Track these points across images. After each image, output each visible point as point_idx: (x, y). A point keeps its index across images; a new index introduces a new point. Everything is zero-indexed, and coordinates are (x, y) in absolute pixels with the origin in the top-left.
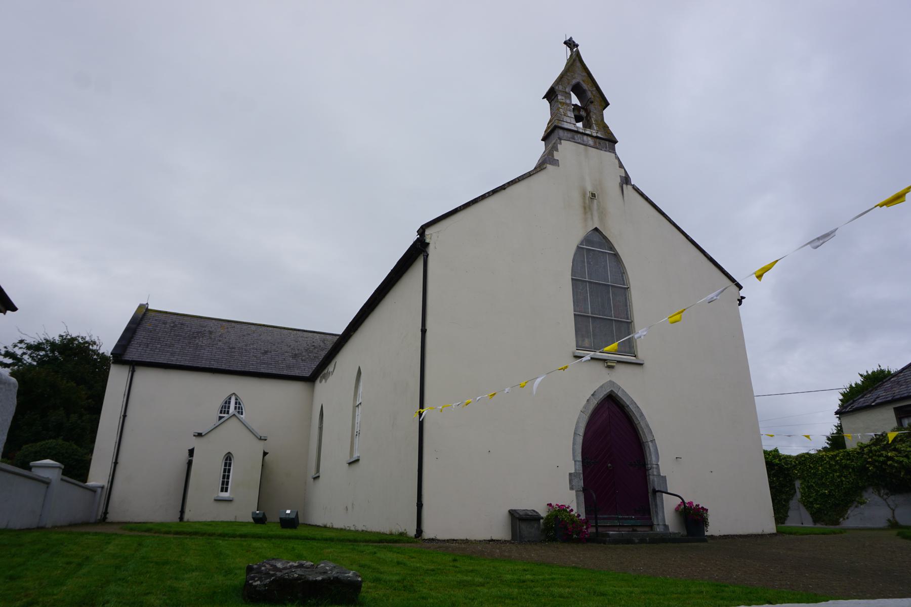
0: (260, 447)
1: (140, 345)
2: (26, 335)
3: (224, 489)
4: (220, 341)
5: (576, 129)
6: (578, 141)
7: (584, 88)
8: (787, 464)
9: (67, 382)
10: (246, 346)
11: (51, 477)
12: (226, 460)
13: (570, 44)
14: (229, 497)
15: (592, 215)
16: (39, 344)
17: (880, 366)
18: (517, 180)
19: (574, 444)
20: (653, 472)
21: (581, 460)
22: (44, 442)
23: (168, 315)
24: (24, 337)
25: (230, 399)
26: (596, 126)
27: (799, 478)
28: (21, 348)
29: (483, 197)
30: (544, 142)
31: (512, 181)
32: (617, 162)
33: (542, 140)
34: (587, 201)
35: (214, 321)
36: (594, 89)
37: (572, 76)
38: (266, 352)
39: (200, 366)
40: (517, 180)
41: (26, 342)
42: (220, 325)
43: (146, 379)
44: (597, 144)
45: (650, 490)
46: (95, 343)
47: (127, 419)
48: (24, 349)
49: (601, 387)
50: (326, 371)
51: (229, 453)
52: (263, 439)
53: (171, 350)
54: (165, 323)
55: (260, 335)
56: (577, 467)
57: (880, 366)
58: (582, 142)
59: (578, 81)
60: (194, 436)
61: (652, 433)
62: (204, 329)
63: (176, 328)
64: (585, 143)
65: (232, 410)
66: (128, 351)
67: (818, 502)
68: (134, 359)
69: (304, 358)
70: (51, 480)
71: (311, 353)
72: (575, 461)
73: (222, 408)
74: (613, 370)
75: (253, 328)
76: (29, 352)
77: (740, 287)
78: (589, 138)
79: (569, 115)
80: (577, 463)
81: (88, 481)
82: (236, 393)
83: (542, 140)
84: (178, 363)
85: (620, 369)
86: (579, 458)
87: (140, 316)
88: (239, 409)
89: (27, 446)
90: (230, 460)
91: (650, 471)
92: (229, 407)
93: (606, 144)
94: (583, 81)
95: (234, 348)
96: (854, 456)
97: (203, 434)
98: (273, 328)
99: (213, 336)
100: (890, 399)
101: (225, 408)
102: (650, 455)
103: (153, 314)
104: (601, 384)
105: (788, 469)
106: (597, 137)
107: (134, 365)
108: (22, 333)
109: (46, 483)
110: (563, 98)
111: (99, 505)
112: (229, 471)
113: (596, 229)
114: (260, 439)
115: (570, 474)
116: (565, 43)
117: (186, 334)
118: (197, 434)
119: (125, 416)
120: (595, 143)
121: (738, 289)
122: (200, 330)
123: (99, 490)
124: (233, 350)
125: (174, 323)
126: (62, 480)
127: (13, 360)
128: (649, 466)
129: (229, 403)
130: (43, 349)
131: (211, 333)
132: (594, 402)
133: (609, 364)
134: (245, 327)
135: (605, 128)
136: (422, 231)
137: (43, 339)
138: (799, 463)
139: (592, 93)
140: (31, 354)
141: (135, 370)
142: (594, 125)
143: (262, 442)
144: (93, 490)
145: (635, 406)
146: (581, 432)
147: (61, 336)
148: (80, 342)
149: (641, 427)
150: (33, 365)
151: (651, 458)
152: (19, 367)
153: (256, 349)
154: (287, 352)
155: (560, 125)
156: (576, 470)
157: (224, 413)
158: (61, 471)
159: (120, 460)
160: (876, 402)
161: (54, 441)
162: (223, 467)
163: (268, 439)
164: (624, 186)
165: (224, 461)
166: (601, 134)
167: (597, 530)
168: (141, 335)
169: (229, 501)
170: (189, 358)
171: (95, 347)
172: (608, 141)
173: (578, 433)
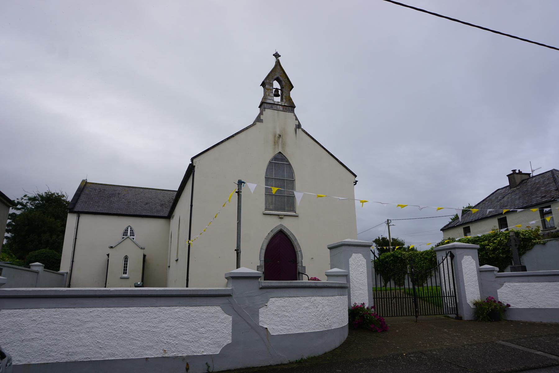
0: (141, 253)
1: (82, 202)
2: (28, 192)
3: (125, 272)
4: (123, 198)
5: (273, 103)
6: (274, 109)
7: (281, 80)
8: (404, 257)
9: (50, 218)
10: (137, 200)
11: (39, 270)
12: (125, 259)
13: (277, 55)
14: (127, 277)
15: (278, 146)
16: (35, 197)
17: (469, 204)
18: (240, 132)
19: (260, 253)
20: (299, 265)
21: (264, 260)
22: (40, 251)
23: (97, 185)
24: (26, 194)
25: (128, 228)
26: (285, 100)
27: (409, 264)
28: (25, 200)
29: (222, 142)
30: (259, 108)
31: (237, 133)
32: (294, 117)
33: (259, 107)
34: (276, 139)
35: (121, 187)
36: (286, 79)
37: (275, 74)
38: (147, 204)
39: (111, 213)
40: (240, 132)
41: (27, 196)
42: (124, 190)
43: (84, 219)
44: (285, 109)
45: (298, 273)
46: (64, 196)
47: (77, 240)
48: (27, 200)
49: (276, 227)
50: (173, 215)
51: (126, 256)
52: (143, 249)
53: (98, 204)
54: (95, 190)
55: (145, 194)
56: (261, 263)
57: (469, 204)
58: (276, 109)
59: (278, 76)
60: (109, 248)
61: (300, 247)
62: (116, 192)
63: (101, 192)
64: (278, 109)
65: (129, 234)
66: (76, 206)
67: (415, 276)
68: (79, 210)
69: (166, 206)
70: (39, 271)
71: (170, 203)
72: (260, 261)
73: (124, 233)
74: (283, 219)
75: (142, 190)
76: (30, 202)
77: (356, 176)
78: (280, 107)
79: (271, 95)
80: (261, 261)
81: (60, 270)
82: (131, 226)
83: (259, 107)
84: (101, 212)
85: (286, 219)
86: (263, 259)
87: (83, 187)
88: (132, 233)
89: (31, 253)
90: (127, 259)
91: (298, 264)
92: (127, 233)
93: (289, 108)
94: (281, 76)
95: (130, 202)
96: (429, 254)
97: (113, 247)
98: (152, 190)
99: (120, 196)
100: (477, 219)
101: (125, 233)
102: (299, 257)
103: (89, 185)
104: (276, 226)
105: (404, 260)
106: (285, 106)
107: (79, 213)
108: (25, 192)
109: (37, 272)
110: (269, 86)
111: (66, 281)
112: (127, 264)
113: (280, 153)
114: (142, 248)
115: (258, 266)
116: (274, 55)
117: (106, 195)
118: (110, 247)
119: (76, 239)
120: (283, 108)
121: (355, 177)
122: (113, 193)
123: (65, 274)
124: (130, 203)
125: (100, 189)
126: (44, 270)
127: (22, 206)
128: (298, 262)
129: (127, 230)
130: (38, 200)
131: (119, 194)
132: (272, 234)
133: (280, 217)
134: (137, 190)
135: (290, 100)
136: (192, 159)
137: (37, 194)
138: (409, 256)
139: (285, 82)
140: (31, 203)
141: (80, 216)
142: (284, 99)
143: (142, 250)
144: (62, 274)
145: (292, 235)
146: (265, 247)
147: (46, 193)
148: (56, 196)
149: (295, 245)
150: (32, 208)
151: (299, 259)
152: (25, 210)
153: (142, 202)
154: (158, 203)
155: (265, 101)
156: (260, 264)
157: (125, 236)
158: (43, 267)
159: (75, 260)
160: (457, 224)
161: (45, 250)
162: (124, 263)
163: (145, 248)
164: (297, 129)
165: (124, 260)
166: (287, 104)
167: (400, 288)
168: (83, 197)
169: (127, 278)
170: (106, 209)
171: (64, 198)
172: (290, 107)
173: (263, 248)
